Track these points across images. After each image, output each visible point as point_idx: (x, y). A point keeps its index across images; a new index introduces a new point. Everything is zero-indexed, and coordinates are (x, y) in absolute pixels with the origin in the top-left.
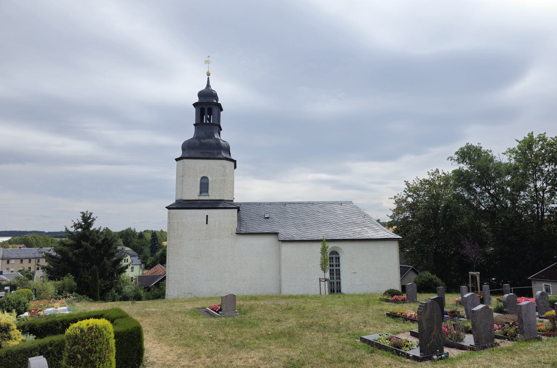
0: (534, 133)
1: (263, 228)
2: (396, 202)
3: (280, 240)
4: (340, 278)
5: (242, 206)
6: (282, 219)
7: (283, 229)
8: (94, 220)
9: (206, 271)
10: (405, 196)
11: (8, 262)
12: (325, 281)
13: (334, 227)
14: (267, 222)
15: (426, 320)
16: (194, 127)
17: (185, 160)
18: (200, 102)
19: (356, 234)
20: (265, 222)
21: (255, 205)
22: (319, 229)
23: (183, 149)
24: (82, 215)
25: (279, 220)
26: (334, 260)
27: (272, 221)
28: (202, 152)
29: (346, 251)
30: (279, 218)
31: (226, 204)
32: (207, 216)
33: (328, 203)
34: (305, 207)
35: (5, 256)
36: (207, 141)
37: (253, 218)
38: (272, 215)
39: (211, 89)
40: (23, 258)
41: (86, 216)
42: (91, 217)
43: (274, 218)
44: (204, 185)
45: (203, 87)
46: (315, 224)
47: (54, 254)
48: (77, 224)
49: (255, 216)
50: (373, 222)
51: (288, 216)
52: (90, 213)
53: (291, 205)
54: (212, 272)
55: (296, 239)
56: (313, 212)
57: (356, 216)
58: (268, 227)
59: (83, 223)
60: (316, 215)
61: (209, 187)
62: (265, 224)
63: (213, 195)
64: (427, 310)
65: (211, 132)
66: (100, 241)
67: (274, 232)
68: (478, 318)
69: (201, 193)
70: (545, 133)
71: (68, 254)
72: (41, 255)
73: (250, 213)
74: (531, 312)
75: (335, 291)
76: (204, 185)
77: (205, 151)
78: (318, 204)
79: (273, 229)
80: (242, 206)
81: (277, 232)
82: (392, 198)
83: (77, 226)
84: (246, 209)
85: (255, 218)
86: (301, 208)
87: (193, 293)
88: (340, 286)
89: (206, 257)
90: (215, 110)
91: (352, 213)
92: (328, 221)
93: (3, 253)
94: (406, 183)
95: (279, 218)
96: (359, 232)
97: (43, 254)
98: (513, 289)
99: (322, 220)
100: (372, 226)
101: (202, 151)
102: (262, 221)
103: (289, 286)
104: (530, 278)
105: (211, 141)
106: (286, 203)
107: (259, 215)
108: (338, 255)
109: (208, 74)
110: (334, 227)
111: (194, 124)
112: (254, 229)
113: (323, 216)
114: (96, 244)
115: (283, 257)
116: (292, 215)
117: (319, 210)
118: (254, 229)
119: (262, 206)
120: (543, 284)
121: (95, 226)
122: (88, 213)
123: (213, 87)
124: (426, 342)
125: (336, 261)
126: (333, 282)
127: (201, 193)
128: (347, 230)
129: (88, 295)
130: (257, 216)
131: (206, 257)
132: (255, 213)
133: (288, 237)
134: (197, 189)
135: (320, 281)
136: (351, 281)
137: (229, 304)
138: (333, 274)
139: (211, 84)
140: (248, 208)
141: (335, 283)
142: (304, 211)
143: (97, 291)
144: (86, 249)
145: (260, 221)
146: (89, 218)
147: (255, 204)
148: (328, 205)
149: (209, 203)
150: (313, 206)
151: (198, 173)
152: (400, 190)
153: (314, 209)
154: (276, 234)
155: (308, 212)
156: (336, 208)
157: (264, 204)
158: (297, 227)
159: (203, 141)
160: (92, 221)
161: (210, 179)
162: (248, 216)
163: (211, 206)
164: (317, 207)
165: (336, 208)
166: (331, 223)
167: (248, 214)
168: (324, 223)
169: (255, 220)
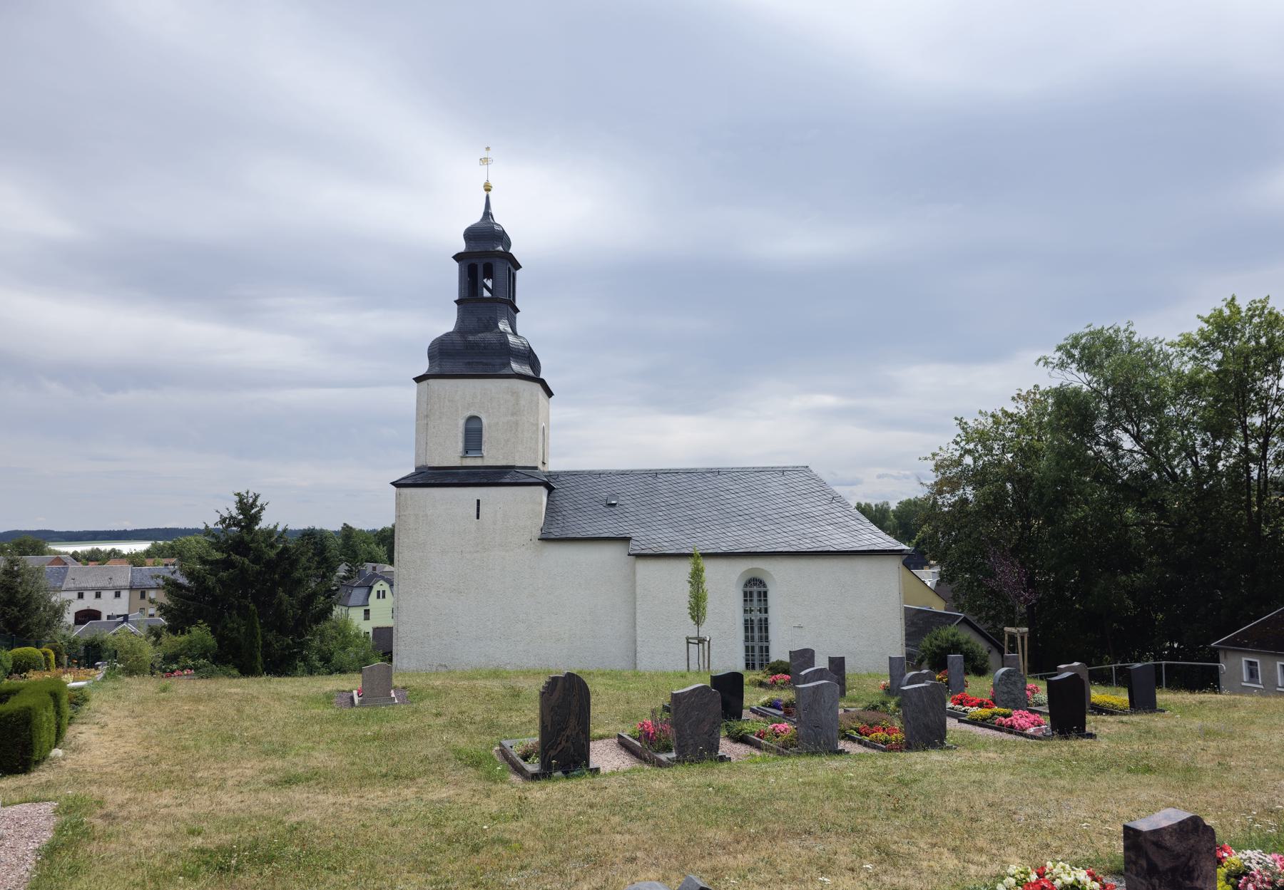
0: (1237, 298)
1: (600, 527)
2: (938, 467)
3: (632, 553)
4: (767, 638)
5: (562, 479)
6: (643, 508)
7: (643, 530)
8: (262, 508)
9: (477, 619)
10: (957, 454)
11: (143, 596)
12: (699, 642)
13: (758, 524)
14: (611, 513)
15: (552, 708)
16: (456, 306)
17: (431, 381)
18: (468, 251)
19: (804, 540)
20: (605, 514)
21: (590, 478)
22: (723, 530)
23: (429, 357)
24: (237, 499)
25: (637, 508)
26: (755, 597)
27: (622, 511)
28: (469, 363)
29: (779, 576)
30: (638, 504)
31: (518, 474)
32: (478, 501)
33: (754, 470)
34: (700, 481)
35: (137, 583)
36: (480, 337)
37: (580, 506)
38: (623, 498)
39: (492, 221)
40: (147, 588)
41: (245, 500)
42: (257, 503)
43: (627, 506)
44: (473, 435)
45: (475, 217)
46: (715, 518)
47: (183, 580)
48: (227, 518)
49: (585, 501)
50: (850, 514)
51: (657, 501)
52: (255, 494)
53: (668, 475)
54: (489, 620)
55: (667, 552)
56: (716, 490)
57: (812, 500)
58: (611, 526)
59: (241, 517)
60: (722, 498)
61: (484, 439)
62: (605, 518)
63: (492, 456)
64: (555, 690)
65: (490, 317)
66: (272, 554)
67: (623, 536)
68: (681, 707)
69: (467, 452)
70: (1268, 296)
71: (205, 580)
72: (153, 583)
73: (576, 495)
74: (824, 702)
75: (757, 666)
76: (473, 435)
77: (474, 360)
78: (730, 472)
79: (621, 529)
80: (562, 479)
81: (628, 536)
82: (926, 459)
83: (227, 521)
84: (568, 485)
85: (585, 505)
86: (690, 483)
87: (450, 664)
88: (768, 655)
89: (477, 588)
90: (500, 268)
91: (805, 492)
92: (747, 512)
93: (132, 576)
94: (958, 422)
95: (638, 504)
96: (811, 535)
97: (161, 582)
98: (1166, 665)
99: (734, 509)
100: (846, 523)
101: (468, 361)
102: (600, 511)
103: (653, 653)
104: (1217, 644)
105: (489, 337)
106: (658, 472)
107: (596, 499)
108: (765, 586)
109: (488, 188)
110: (758, 524)
111: (455, 301)
112: (579, 530)
113: (738, 499)
114: (264, 561)
115: (638, 591)
116: (668, 499)
117: (732, 488)
118: (579, 530)
119: (604, 479)
120: (1244, 659)
121: (265, 523)
122: (251, 494)
123: (502, 219)
124: (547, 747)
125: (760, 600)
126: (753, 647)
127: (467, 452)
128: (785, 530)
129: (236, 666)
130: (592, 500)
131: (477, 588)
132: (587, 493)
133: (650, 546)
134: (457, 442)
135: (688, 643)
136: (791, 643)
137: (377, 683)
138: (752, 628)
139: (493, 210)
140: (573, 484)
141: (757, 649)
142: (695, 490)
143: (255, 658)
144: (243, 571)
145: (595, 512)
146: (253, 505)
147: (590, 473)
148: (752, 475)
149: (483, 472)
150: (719, 477)
151: (460, 408)
152: (945, 442)
153: (720, 485)
154: (627, 540)
155: (705, 492)
156: (769, 481)
157: (610, 474)
158: (676, 524)
159: (471, 338)
160: (259, 512)
161: (484, 421)
162: (571, 500)
163: (485, 481)
164: (726, 480)
165: (769, 481)
166: (753, 516)
167: (571, 496)
168: (736, 515)
169: (585, 510)
